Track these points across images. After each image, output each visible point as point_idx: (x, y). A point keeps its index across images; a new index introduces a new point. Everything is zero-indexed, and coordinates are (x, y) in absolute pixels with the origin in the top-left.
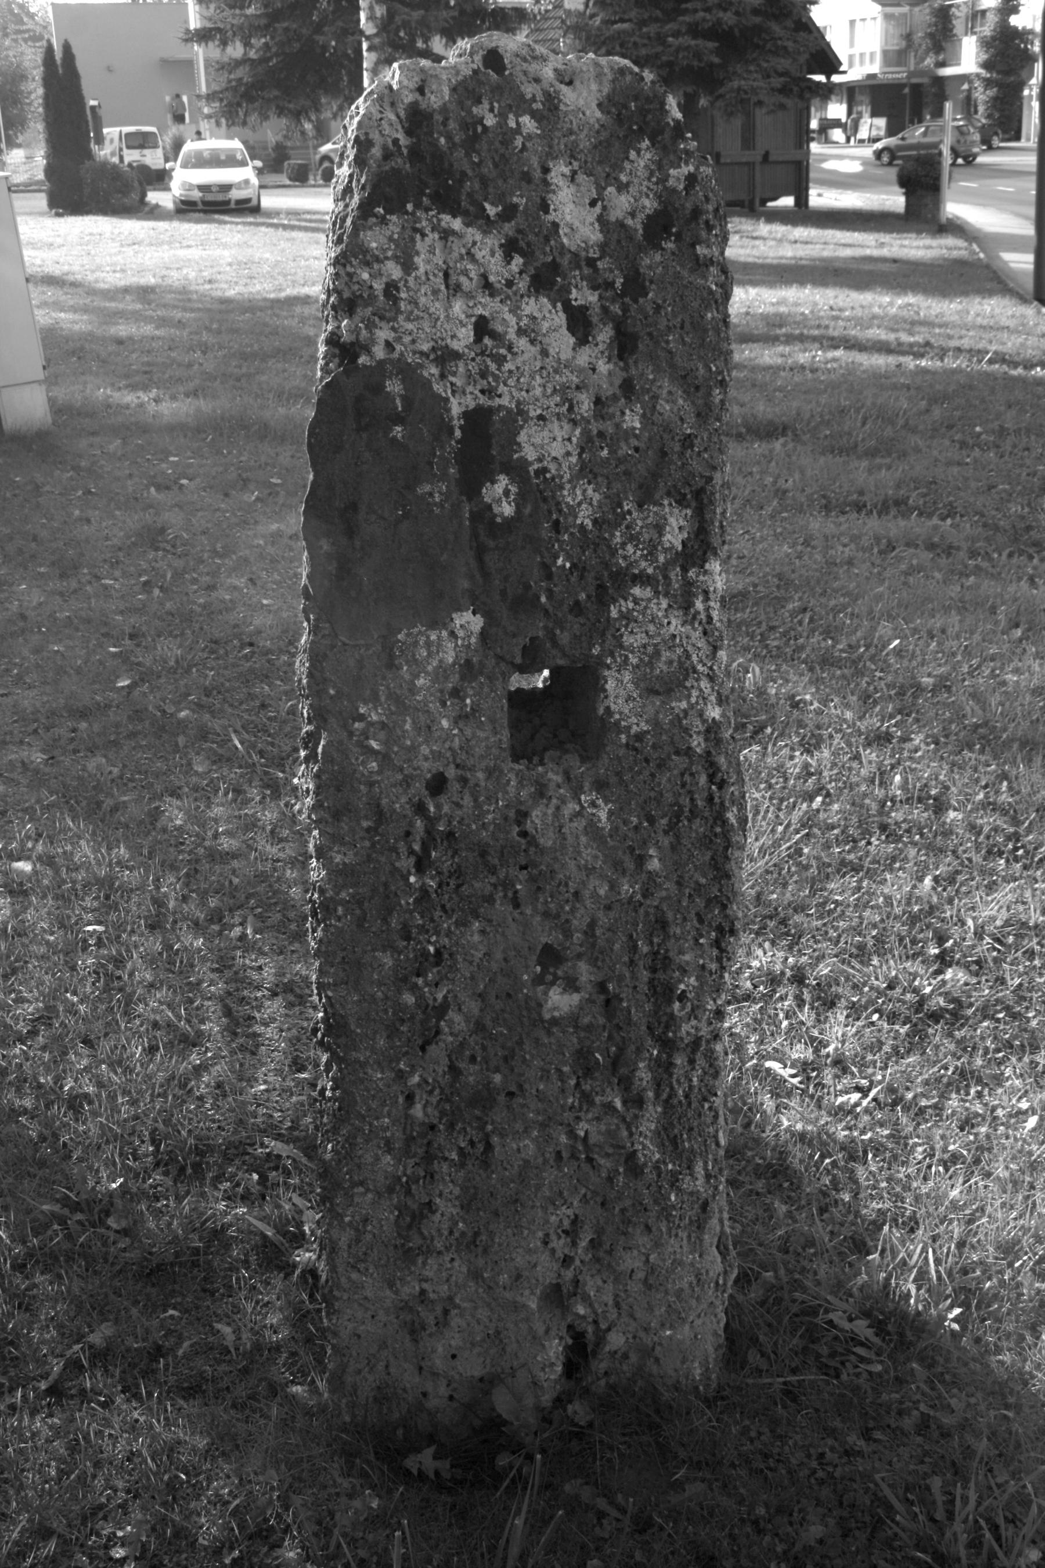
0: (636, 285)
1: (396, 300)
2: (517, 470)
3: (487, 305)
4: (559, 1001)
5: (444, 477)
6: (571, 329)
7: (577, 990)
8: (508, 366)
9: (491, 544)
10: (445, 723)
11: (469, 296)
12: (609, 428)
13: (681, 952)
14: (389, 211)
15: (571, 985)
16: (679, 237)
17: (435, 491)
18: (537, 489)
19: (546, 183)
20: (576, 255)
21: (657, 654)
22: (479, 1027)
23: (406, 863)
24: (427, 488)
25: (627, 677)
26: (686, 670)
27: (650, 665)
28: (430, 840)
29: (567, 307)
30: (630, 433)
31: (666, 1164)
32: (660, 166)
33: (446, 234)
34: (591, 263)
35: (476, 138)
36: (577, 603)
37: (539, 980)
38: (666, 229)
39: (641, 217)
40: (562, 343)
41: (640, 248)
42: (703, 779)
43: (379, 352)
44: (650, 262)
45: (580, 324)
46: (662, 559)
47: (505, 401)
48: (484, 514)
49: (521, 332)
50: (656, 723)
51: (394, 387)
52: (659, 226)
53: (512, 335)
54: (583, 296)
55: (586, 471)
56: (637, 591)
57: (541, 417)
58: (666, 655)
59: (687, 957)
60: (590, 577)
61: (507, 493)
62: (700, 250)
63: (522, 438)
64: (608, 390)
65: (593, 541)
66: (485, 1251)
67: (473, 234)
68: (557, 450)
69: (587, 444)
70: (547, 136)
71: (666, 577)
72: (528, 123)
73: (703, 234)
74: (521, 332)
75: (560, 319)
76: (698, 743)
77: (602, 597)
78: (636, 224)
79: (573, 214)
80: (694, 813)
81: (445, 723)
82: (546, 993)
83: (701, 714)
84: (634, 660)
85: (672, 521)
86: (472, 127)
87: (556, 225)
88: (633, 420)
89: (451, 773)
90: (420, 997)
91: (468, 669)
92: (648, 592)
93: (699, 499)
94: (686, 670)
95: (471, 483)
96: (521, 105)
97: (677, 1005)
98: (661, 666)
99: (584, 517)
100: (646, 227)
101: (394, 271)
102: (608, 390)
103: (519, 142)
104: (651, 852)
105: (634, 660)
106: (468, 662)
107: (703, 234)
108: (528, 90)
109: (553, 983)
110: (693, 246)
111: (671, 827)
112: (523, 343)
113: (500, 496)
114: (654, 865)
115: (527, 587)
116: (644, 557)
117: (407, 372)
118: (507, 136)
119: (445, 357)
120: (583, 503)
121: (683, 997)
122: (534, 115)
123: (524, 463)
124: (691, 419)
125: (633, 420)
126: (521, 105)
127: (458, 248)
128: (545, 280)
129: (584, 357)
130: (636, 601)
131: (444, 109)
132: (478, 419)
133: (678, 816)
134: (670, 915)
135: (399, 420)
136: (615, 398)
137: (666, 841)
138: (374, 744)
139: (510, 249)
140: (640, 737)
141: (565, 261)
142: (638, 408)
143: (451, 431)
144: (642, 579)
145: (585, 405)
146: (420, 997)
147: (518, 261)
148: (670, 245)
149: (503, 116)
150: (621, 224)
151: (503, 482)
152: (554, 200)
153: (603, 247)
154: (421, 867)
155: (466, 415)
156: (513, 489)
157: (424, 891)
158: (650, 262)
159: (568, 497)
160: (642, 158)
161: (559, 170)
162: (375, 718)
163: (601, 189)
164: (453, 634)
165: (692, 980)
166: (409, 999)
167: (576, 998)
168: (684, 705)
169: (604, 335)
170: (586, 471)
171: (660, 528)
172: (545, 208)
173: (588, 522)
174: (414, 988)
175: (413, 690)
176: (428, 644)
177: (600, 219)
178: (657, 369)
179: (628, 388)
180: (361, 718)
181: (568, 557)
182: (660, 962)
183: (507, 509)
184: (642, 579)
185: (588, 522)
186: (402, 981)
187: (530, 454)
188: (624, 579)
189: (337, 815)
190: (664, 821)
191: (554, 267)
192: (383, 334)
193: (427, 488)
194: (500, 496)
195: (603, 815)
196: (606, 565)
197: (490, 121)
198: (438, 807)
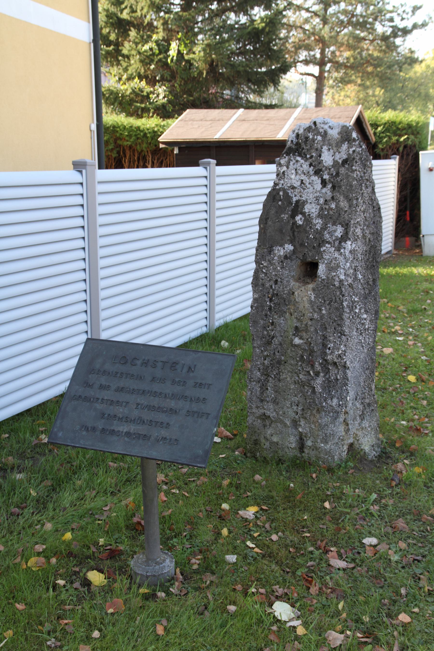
0: (338, 174)
1: (284, 175)
2: (303, 214)
3: (303, 177)
4: (297, 341)
5: (287, 214)
6: (321, 184)
7: (303, 339)
8: (305, 191)
9: (296, 230)
10: (279, 268)
11: (300, 175)
12: (327, 207)
13: (330, 337)
14: (286, 155)
15: (301, 338)
16: (349, 164)
17: (285, 216)
18: (308, 219)
19: (321, 151)
20: (326, 167)
21: (331, 261)
22: (281, 344)
23: (267, 299)
24: (283, 216)
25: (324, 265)
26: (338, 266)
27: (330, 263)
28: (273, 295)
29: (322, 178)
30: (332, 209)
31: (323, 394)
32: (348, 148)
33: (297, 161)
34: (330, 169)
35: (307, 141)
36: (314, 246)
37: (294, 335)
38: (346, 162)
39: (342, 160)
40: (318, 186)
41: (340, 166)
42: (338, 293)
43: (280, 186)
44: (342, 170)
45: (324, 183)
46: (334, 238)
47: (303, 199)
48: (295, 223)
49: (310, 183)
50: (328, 278)
51: (281, 193)
52: (345, 162)
53: (307, 184)
54: (326, 177)
55: (320, 216)
56: (327, 245)
57: (311, 203)
58: (334, 262)
59: (331, 338)
60: (317, 241)
61: (301, 219)
62: (354, 167)
63: (305, 207)
64: (329, 198)
65: (320, 233)
66: (277, 404)
67: (302, 161)
68: (313, 210)
69: (321, 209)
70: (323, 140)
71: (334, 243)
72: (319, 138)
73: (355, 164)
74: (310, 183)
75: (319, 181)
76: (337, 284)
77: (320, 246)
78: (340, 161)
79: (327, 158)
80: (336, 302)
81: (279, 268)
82: (295, 338)
83: (339, 277)
84: (326, 262)
85: (338, 230)
86: (307, 138)
87: (322, 160)
88: (333, 206)
89: (279, 280)
90: (268, 333)
91: (286, 257)
92: (329, 246)
93: (346, 226)
94: (338, 266)
95: (293, 216)
96: (319, 133)
97: (328, 350)
98: (332, 265)
99: (318, 227)
100: (342, 162)
101: (285, 168)
102: (329, 198)
103: (316, 142)
104: (323, 308)
105: (326, 262)
106: (286, 255)
107: (355, 164)
108: (321, 130)
109: (297, 336)
110: (352, 166)
111: (329, 304)
112: (309, 186)
113: (299, 220)
114: (324, 312)
115: (303, 241)
116: (330, 237)
117: (284, 190)
118: (313, 140)
119: (293, 188)
120: (318, 223)
121: (329, 349)
122: (321, 136)
123: (305, 213)
124: (348, 207)
125: (333, 206)
126: (319, 133)
127: (299, 164)
128: (318, 172)
129: (324, 190)
130: (327, 247)
131: (301, 134)
132: (297, 202)
133: (331, 301)
134: (327, 326)
135: (280, 200)
136: (330, 200)
137: (328, 307)
138: (264, 271)
139: (311, 165)
140: (323, 280)
141: (324, 169)
142: (335, 203)
143: (292, 204)
144: (329, 243)
145: (322, 201)
146: (268, 333)
147: (312, 168)
148: (347, 166)
149: (314, 136)
150: (337, 161)
151: (300, 216)
152: (323, 154)
153: (333, 166)
154: (271, 300)
155: (296, 201)
156: (303, 218)
157: (270, 306)
158: (342, 170)
159: (315, 221)
160: (345, 146)
161: (325, 148)
162: (265, 265)
163: (335, 153)
164: (284, 249)
165: (332, 345)
166: (265, 333)
167: (302, 341)
168: (335, 274)
169: (330, 186)
170: (320, 216)
171: (335, 231)
172: (320, 156)
173: (319, 228)
174: (267, 330)
175: (273, 259)
176: (278, 250)
177: (333, 159)
178: (340, 194)
179: (333, 198)
180: (262, 264)
181: (313, 235)
182: (325, 338)
183: (301, 223)
184: (329, 243)
185: (319, 228)
186: (264, 328)
187: (306, 210)
188: (324, 242)
189: (256, 286)
190: (328, 302)
191: (321, 170)
192: (282, 182)
193: (283, 216)
194: (299, 220)
195: (313, 298)
196: (321, 238)
197: (311, 137)
198: (275, 287)
